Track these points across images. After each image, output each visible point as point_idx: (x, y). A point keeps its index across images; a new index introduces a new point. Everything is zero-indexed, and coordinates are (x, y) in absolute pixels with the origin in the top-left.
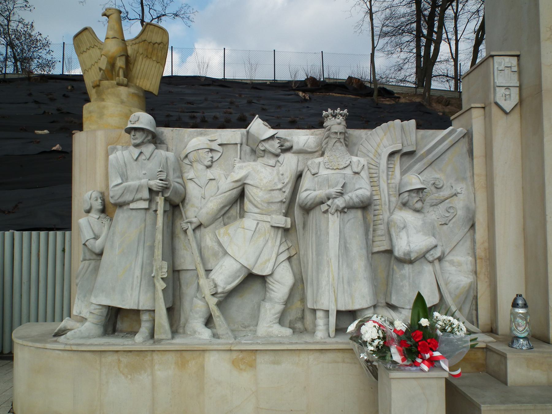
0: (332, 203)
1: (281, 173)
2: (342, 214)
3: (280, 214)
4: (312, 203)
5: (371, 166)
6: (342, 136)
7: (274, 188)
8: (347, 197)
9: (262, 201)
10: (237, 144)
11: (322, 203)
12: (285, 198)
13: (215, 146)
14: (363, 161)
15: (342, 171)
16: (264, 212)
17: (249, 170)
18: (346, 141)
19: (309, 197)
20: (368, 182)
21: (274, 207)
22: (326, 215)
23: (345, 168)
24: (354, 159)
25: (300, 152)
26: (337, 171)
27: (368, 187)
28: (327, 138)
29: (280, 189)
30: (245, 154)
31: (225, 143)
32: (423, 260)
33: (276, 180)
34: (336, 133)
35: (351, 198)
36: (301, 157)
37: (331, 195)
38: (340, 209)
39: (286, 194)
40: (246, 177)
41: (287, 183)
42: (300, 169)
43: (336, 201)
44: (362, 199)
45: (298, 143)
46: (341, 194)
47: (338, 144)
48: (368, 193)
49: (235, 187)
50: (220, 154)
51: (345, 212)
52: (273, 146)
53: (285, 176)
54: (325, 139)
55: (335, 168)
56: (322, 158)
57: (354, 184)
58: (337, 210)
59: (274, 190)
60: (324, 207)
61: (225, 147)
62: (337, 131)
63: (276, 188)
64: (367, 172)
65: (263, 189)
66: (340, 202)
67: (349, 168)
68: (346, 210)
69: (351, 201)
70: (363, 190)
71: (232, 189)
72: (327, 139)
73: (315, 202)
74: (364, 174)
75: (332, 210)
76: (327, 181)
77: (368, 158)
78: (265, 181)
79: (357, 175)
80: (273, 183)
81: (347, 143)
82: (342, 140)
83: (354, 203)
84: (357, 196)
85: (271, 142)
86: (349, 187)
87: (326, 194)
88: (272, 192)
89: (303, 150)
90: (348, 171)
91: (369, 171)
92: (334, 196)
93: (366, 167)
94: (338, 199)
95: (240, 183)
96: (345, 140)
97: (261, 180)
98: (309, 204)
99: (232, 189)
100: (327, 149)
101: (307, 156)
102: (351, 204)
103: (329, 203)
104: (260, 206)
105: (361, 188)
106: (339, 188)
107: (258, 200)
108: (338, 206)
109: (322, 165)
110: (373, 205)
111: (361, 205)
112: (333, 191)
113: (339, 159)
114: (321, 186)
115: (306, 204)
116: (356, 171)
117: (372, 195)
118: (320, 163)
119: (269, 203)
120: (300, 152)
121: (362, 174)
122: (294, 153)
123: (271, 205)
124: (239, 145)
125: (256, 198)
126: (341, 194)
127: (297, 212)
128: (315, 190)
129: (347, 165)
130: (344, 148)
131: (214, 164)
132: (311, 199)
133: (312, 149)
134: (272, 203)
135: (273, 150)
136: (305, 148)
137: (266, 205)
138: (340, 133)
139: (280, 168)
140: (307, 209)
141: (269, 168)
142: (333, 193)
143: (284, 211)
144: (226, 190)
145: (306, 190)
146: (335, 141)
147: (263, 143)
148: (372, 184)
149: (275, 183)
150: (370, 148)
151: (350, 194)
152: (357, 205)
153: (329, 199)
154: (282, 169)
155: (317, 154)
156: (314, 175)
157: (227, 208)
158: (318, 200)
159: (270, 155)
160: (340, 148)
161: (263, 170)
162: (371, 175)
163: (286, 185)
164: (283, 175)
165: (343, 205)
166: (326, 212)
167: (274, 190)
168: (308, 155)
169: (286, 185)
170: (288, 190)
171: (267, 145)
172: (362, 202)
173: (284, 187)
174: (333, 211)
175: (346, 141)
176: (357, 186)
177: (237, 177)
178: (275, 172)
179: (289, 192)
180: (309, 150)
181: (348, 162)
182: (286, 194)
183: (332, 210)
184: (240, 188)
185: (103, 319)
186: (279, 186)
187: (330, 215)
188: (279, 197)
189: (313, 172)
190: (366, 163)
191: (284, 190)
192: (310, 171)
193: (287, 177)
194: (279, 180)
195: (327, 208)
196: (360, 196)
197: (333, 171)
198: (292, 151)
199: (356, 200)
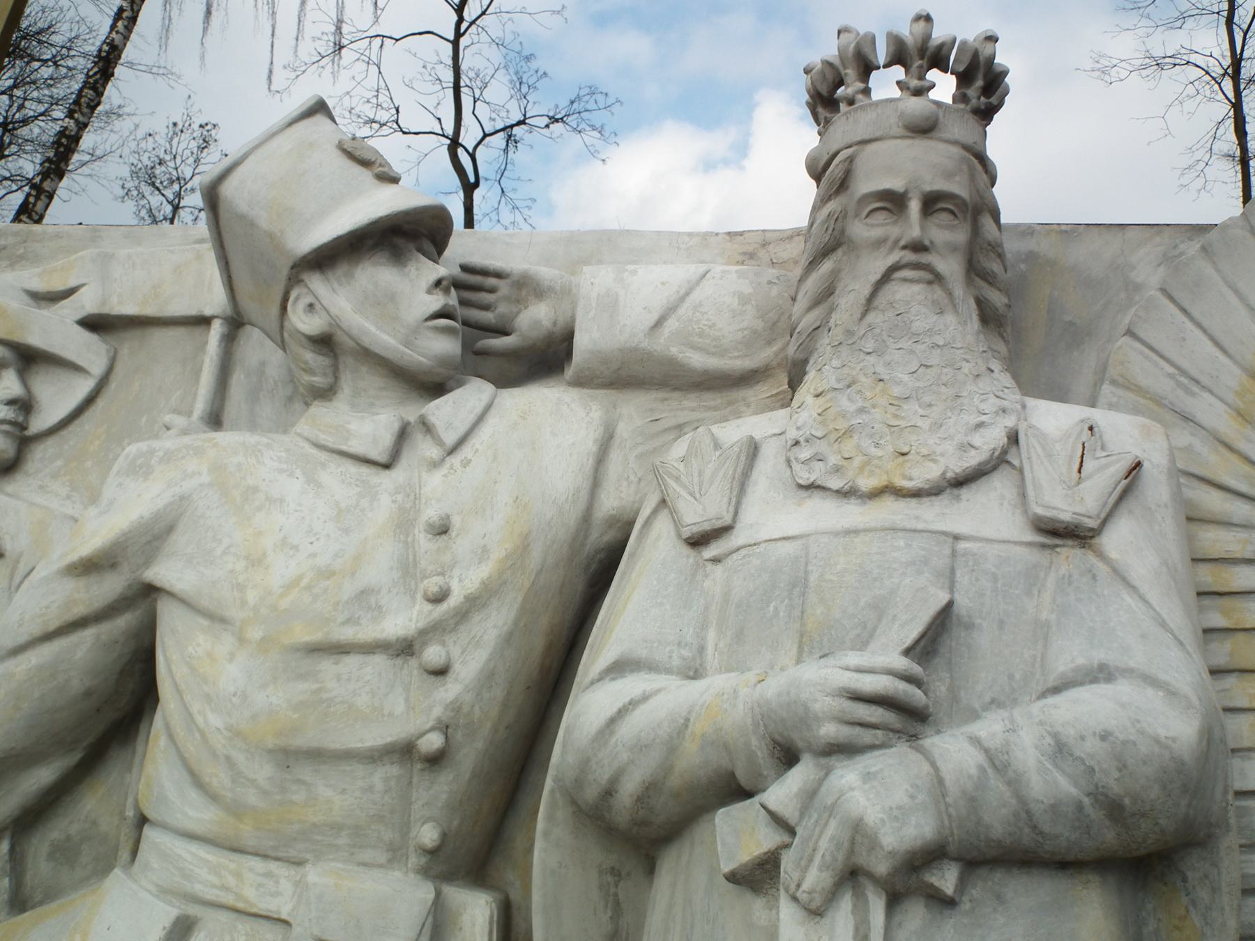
0: (810, 796)
1: (431, 513)
2: (915, 915)
3: (396, 854)
4: (651, 788)
5: (1213, 501)
6: (947, 234)
7: (347, 634)
8: (955, 750)
9: (235, 733)
10: (203, 321)
11: (735, 790)
12: (444, 728)
13: (55, 331)
14: (1127, 433)
15: (933, 514)
16: (247, 833)
17: (187, 486)
18: (988, 278)
19: (628, 730)
20: (1175, 612)
21: (337, 796)
22: (758, 906)
23: (961, 482)
24: (1053, 419)
25: (629, 375)
26: (890, 511)
27: (1182, 668)
28: (825, 252)
29: (405, 648)
30: (254, 396)
31: (129, 309)
32: (1004, 466)
33: (379, 568)
34: (893, 202)
35: (997, 762)
36: (633, 411)
37: (806, 719)
38: (882, 868)
39: (451, 690)
40: (155, 535)
41: (474, 603)
42: (610, 502)
43: (847, 777)
44: (1113, 784)
45: (610, 304)
46: (904, 717)
47: (907, 293)
48: (1178, 727)
49: (79, 610)
50: (83, 387)
51: (946, 903)
52: (384, 304)
53: (461, 544)
54: (813, 264)
55: (867, 483)
56: (782, 413)
57: (1042, 633)
58: (851, 876)
59: (341, 649)
60: (737, 834)
61: (128, 345)
62: (896, 184)
63: (368, 632)
64: (1168, 525)
65: (255, 633)
66: (883, 798)
67: (999, 487)
68: (946, 879)
69: (998, 788)
70: (1123, 689)
71: (48, 637)
72: (827, 266)
73: (675, 781)
74: (1138, 546)
75: (808, 872)
76: (796, 605)
77: (1184, 437)
78: (281, 570)
79: (1070, 557)
80: (349, 589)
81: (997, 298)
82: (950, 266)
83: (1025, 813)
84: (1060, 750)
85: (375, 275)
86: (988, 655)
87: (764, 716)
88: (328, 667)
89: (645, 357)
90: (989, 516)
91: (1190, 539)
92: (829, 731)
93: (1156, 488)
94: (871, 761)
95: (109, 587)
96: (974, 271)
97: (257, 561)
98: (630, 787)
99: (48, 637)
100: (824, 343)
101: (686, 406)
102: (997, 820)
103: (783, 793)
104: (218, 777)
105: (1101, 674)
106: (880, 661)
107: (215, 721)
108: (857, 828)
109: (769, 463)
110: (1229, 842)
111: (1108, 837)
112: (819, 682)
113: (911, 408)
114: (739, 637)
115: (609, 792)
116: (1062, 505)
117: (1215, 748)
118: (753, 450)
119: (295, 757)
120: (629, 375)
121: (1120, 540)
122: (581, 382)
123: (305, 772)
124: (217, 329)
125: (195, 707)
126: (907, 717)
127: (550, 850)
128: (693, 672)
129: (973, 460)
130: (958, 328)
131: (39, 455)
132: (640, 747)
133: (722, 353)
134: (317, 756)
135: (385, 340)
136: (667, 344)
137: (263, 772)
138: (932, 203)
139: (434, 482)
140: (641, 834)
141: (339, 481)
142: (824, 704)
143: (428, 835)
144: (22, 639)
145: (619, 668)
146: (876, 265)
147: (316, 283)
148: (1223, 652)
149: (364, 594)
150: (1198, 352)
151: (990, 727)
152: (1063, 835)
153: (788, 757)
154: (437, 487)
155: (762, 391)
156: (698, 541)
157: (43, 776)
158: (693, 760)
159: (371, 381)
160: (923, 319)
161: (292, 487)
162: (1208, 577)
163: (463, 615)
164: (442, 530)
165: (920, 829)
166: (759, 876)
167: (341, 649)
168: (691, 401)
169: (463, 615)
170: (478, 659)
171: (342, 301)
172: (1114, 809)
173: (429, 632)
174: (815, 878)
175: (988, 278)
176: (1069, 654)
177: (97, 532)
178: (383, 509)
179: (487, 677)
180: (698, 360)
181: (992, 438)
182: (451, 690)
183: (808, 872)
184: (124, 622)
185: (919, 843)
186: (400, 620)
187: (787, 912)
188: (401, 710)
189: (696, 516)
190: (1156, 459)
191: (433, 654)
192: (673, 513)
193: (483, 553)
194: (408, 569)
195: (763, 840)
196: (1092, 746)
197: (853, 514)
198: (569, 372)
199: (1049, 785)
